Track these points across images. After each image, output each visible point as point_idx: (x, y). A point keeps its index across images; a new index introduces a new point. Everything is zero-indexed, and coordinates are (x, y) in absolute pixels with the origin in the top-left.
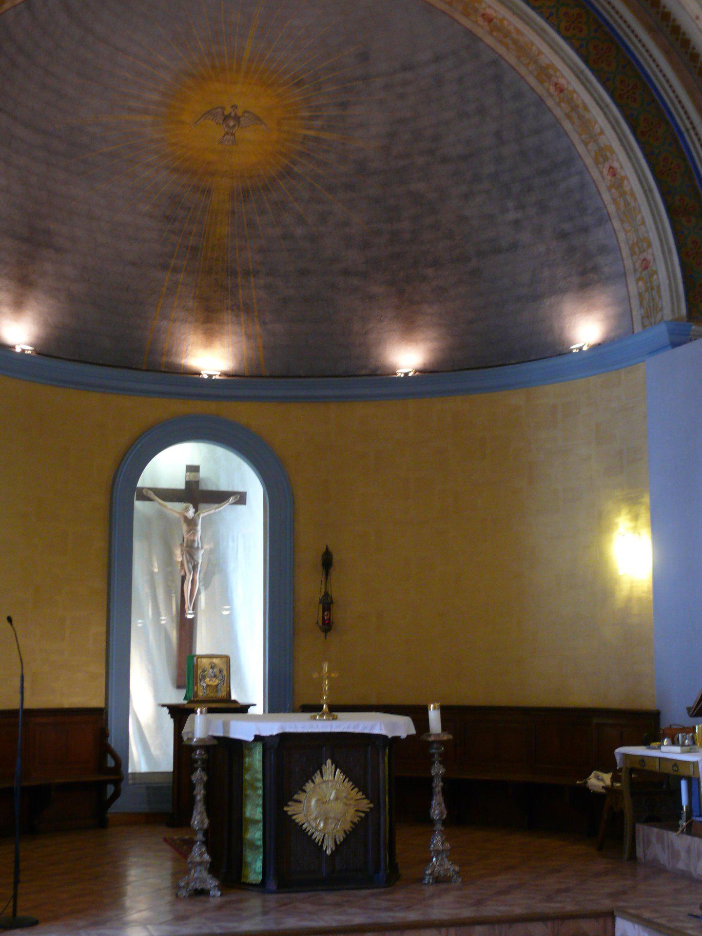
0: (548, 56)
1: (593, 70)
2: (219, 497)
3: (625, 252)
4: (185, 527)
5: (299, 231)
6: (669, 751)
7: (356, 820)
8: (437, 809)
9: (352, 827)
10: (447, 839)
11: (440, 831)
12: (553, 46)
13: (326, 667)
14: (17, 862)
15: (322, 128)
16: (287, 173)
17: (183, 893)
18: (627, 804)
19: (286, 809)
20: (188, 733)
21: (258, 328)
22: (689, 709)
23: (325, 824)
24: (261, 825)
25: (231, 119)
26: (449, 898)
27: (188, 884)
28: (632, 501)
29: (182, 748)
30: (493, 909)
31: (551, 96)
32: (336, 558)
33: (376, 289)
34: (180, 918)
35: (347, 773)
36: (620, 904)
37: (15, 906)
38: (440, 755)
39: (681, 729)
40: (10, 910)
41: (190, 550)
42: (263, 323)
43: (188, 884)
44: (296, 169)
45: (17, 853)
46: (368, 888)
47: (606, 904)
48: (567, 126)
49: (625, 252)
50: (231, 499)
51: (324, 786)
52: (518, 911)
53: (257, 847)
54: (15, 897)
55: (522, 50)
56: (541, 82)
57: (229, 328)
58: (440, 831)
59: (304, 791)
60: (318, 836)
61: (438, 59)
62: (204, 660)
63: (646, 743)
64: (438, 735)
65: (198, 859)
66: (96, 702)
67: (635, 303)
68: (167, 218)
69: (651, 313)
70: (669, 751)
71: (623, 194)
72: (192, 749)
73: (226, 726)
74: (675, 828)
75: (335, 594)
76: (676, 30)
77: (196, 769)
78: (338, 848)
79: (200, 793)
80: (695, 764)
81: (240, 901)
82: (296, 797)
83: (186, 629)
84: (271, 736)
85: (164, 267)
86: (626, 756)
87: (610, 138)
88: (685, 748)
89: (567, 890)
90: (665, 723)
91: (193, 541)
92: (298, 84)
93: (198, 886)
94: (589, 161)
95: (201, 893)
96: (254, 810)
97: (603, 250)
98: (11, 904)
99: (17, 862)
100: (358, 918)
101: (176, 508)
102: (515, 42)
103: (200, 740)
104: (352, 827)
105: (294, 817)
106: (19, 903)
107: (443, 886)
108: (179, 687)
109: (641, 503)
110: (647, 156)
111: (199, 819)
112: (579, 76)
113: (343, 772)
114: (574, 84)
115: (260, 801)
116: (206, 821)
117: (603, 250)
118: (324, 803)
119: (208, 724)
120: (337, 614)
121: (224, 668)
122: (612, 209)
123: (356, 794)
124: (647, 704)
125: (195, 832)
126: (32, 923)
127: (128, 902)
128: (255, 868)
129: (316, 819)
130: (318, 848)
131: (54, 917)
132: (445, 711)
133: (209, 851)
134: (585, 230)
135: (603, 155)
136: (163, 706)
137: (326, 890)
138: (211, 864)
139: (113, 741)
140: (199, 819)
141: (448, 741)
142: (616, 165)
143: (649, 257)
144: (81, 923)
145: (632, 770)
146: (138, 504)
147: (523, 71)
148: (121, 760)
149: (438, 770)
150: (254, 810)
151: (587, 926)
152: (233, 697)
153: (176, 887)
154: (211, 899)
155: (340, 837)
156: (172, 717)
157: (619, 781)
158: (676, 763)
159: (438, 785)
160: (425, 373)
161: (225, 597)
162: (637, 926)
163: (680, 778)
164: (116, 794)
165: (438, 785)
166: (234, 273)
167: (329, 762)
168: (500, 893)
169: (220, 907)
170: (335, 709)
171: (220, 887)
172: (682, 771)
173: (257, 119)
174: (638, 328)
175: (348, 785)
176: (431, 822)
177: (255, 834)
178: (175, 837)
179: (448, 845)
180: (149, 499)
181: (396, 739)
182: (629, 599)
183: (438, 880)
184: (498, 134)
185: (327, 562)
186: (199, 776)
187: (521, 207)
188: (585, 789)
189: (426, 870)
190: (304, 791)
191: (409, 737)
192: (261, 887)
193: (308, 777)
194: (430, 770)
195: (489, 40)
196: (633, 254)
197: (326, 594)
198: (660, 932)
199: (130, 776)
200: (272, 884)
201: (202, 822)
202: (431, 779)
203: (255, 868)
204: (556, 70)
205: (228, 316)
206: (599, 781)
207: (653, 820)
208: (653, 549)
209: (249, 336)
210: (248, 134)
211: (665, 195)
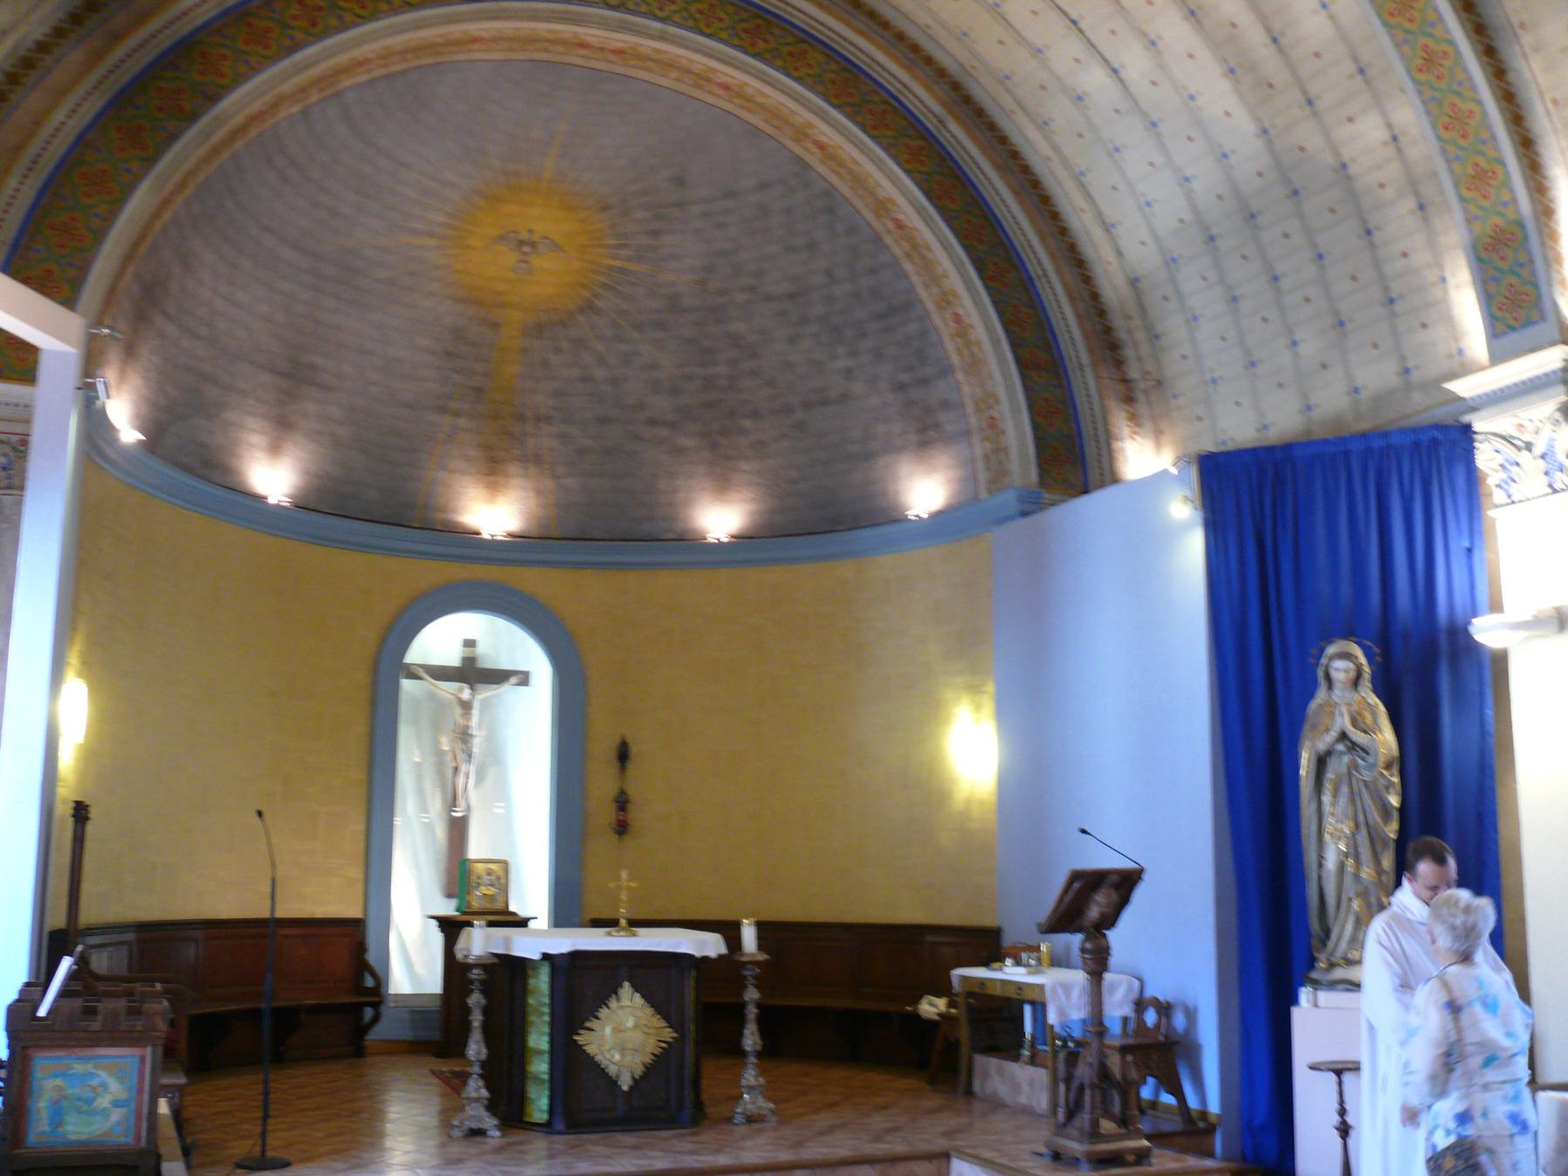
0: (887, 189)
1: (936, 207)
2: (498, 677)
3: (970, 408)
4: (458, 711)
5: (600, 373)
6: (1011, 972)
7: (657, 1051)
8: (751, 1039)
9: (653, 1060)
10: (762, 1071)
11: (754, 1064)
12: (895, 182)
13: (624, 874)
14: (266, 1093)
15: (629, 259)
16: (588, 307)
17: (457, 1133)
18: (964, 1033)
19: (576, 1038)
20: (462, 949)
21: (549, 484)
22: (1039, 925)
23: (622, 1055)
24: (546, 1057)
25: (526, 245)
26: (761, 1140)
27: (462, 1123)
28: (975, 689)
29: (454, 969)
30: (813, 1152)
31: (889, 232)
32: (634, 749)
33: (687, 442)
34: (452, 1162)
35: (648, 998)
36: (954, 1143)
37: (264, 1145)
38: (756, 977)
39: (1024, 948)
40: (258, 1149)
41: (464, 736)
42: (555, 477)
43: (462, 1123)
44: (599, 303)
45: (266, 1082)
46: (670, 1129)
47: (941, 1144)
48: (908, 266)
49: (970, 408)
50: (513, 680)
51: (620, 1012)
52: (843, 1153)
53: (542, 1081)
54: (263, 1135)
55: (858, 181)
56: (878, 216)
57: (517, 481)
58: (754, 1064)
59: (597, 1018)
60: (612, 1070)
61: (764, 186)
62: (480, 867)
63: (986, 963)
64: (752, 955)
65: (474, 1095)
66: (353, 912)
67: (980, 465)
68: (448, 354)
69: (998, 478)
70: (1011, 972)
71: (968, 344)
72: (467, 967)
73: (508, 941)
74: (1016, 1058)
75: (632, 791)
76: (1026, 170)
77: (472, 991)
78: (637, 1083)
79: (477, 1019)
80: (1041, 987)
81: (521, 1143)
82: (588, 1024)
83: (458, 830)
84: (562, 955)
85: (443, 410)
86: (965, 979)
87: (955, 282)
88: (1032, 969)
89: (896, 1129)
90: (1008, 940)
91: (467, 727)
92: (605, 209)
93: (475, 1125)
94: (931, 306)
95: (477, 1133)
96: (539, 1039)
97: (946, 405)
98: (259, 1142)
99: (266, 1093)
100: (661, 1163)
101: (448, 688)
102: (851, 172)
103: (479, 957)
104: (653, 1060)
105: (584, 1048)
106: (269, 1141)
107: (756, 1126)
108: (449, 895)
109: (984, 692)
110: (995, 303)
111: (476, 1048)
112: (920, 210)
113: (643, 996)
114: (918, 223)
115: (546, 1029)
116: (484, 1051)
117: (946, 405)
118: (620, 1031)
119: (488, 938)
120: (635, 816)
121: (501, 874)
122: (955, 359)
123: (658, 1022)
124: (988, 921)
125: (470, 1063)
126: (285, 1164)
127: (389, 1143)
128: (539, 1104)
129: (611, 1048)
130: (613, 1083)
131: (309, 1159)
132: (763, 928)
133: (488, 1087)
134: (924, 382)
135: (946, 300)
136: (433, 917)
137: (624, 1131)
138: (490, 1100)
139: (372, 957)
140: (476, 1048)
141: (766, 961)
142: (961, 311)
143: (996, 415)
144: (339, 1165)
145: (970, 994)
146: (406, 684)
147: (858, 204)
148: (381, 981)
149: (752, 994)
150: (539, 1039)
151: (923, 1168)
152: (512, 908)
153: (446, 1125)
154: (488, 1140)
155: (639, 1071)
156: (442, 932)
157: (954, 1007)
158: (1020, 986)
159: (752, 1012)
160: (742, 540)
161: (502, 792)
162: (974, 1167)
163: (1021, 1003)
164: (376, 1019)
165: (752, 1012)
166: (521, 418)
167: (626, 984)
168: (821, 1133)
169: (499, 1150)
170: (635, 923)
171: (499, 1127)
172: (1028, 995)
173: (557, 247)
174: (983, 494)
175: (649, 1011)
176: (741, 1053)
177: (540, 1067)
178: (444, 1069)
179: (762, 1080)
180: (417, 677)
181: (705, 959)
182: (969, 801)
183: (751, 1119)
184: (829, 273)
185: (623, 754)
186: (476, 999)
187: (853, 354)
188: (916, 1017)
189: (737, 1108)
190: (597, 1018)
191: (721, 957)
192: (547, 1127)
193: (603, 1001)
194: (741, 995)
195: (821, 169)
196: (978, 410)
197: (622, 792)
198: (1000, 1172)
199: (390, 998)
200: (560, 1126)
201: (479, 1053)
202: (743, 1005)
203: (539, 1104)
204: (895, 204)
205: (514, 468)
206: (931, 1007)
207: (992, 1050)
208: (998, 736)
209: (539, 492)
210: (545, 263)
211: (1015, 345)
